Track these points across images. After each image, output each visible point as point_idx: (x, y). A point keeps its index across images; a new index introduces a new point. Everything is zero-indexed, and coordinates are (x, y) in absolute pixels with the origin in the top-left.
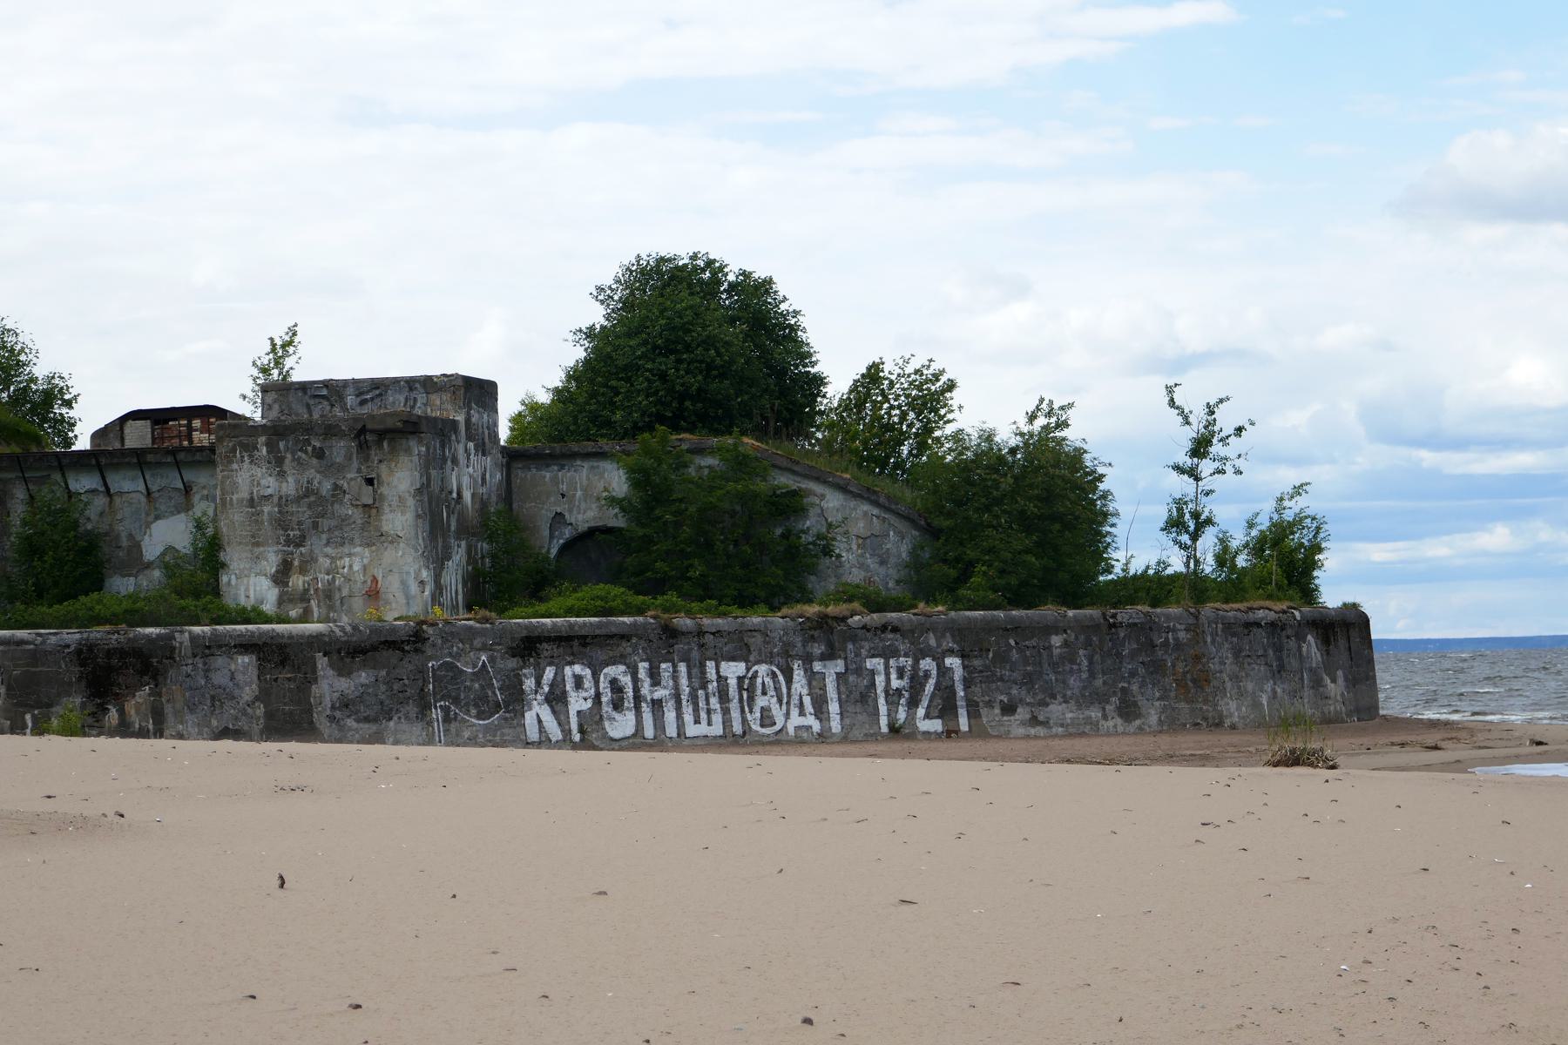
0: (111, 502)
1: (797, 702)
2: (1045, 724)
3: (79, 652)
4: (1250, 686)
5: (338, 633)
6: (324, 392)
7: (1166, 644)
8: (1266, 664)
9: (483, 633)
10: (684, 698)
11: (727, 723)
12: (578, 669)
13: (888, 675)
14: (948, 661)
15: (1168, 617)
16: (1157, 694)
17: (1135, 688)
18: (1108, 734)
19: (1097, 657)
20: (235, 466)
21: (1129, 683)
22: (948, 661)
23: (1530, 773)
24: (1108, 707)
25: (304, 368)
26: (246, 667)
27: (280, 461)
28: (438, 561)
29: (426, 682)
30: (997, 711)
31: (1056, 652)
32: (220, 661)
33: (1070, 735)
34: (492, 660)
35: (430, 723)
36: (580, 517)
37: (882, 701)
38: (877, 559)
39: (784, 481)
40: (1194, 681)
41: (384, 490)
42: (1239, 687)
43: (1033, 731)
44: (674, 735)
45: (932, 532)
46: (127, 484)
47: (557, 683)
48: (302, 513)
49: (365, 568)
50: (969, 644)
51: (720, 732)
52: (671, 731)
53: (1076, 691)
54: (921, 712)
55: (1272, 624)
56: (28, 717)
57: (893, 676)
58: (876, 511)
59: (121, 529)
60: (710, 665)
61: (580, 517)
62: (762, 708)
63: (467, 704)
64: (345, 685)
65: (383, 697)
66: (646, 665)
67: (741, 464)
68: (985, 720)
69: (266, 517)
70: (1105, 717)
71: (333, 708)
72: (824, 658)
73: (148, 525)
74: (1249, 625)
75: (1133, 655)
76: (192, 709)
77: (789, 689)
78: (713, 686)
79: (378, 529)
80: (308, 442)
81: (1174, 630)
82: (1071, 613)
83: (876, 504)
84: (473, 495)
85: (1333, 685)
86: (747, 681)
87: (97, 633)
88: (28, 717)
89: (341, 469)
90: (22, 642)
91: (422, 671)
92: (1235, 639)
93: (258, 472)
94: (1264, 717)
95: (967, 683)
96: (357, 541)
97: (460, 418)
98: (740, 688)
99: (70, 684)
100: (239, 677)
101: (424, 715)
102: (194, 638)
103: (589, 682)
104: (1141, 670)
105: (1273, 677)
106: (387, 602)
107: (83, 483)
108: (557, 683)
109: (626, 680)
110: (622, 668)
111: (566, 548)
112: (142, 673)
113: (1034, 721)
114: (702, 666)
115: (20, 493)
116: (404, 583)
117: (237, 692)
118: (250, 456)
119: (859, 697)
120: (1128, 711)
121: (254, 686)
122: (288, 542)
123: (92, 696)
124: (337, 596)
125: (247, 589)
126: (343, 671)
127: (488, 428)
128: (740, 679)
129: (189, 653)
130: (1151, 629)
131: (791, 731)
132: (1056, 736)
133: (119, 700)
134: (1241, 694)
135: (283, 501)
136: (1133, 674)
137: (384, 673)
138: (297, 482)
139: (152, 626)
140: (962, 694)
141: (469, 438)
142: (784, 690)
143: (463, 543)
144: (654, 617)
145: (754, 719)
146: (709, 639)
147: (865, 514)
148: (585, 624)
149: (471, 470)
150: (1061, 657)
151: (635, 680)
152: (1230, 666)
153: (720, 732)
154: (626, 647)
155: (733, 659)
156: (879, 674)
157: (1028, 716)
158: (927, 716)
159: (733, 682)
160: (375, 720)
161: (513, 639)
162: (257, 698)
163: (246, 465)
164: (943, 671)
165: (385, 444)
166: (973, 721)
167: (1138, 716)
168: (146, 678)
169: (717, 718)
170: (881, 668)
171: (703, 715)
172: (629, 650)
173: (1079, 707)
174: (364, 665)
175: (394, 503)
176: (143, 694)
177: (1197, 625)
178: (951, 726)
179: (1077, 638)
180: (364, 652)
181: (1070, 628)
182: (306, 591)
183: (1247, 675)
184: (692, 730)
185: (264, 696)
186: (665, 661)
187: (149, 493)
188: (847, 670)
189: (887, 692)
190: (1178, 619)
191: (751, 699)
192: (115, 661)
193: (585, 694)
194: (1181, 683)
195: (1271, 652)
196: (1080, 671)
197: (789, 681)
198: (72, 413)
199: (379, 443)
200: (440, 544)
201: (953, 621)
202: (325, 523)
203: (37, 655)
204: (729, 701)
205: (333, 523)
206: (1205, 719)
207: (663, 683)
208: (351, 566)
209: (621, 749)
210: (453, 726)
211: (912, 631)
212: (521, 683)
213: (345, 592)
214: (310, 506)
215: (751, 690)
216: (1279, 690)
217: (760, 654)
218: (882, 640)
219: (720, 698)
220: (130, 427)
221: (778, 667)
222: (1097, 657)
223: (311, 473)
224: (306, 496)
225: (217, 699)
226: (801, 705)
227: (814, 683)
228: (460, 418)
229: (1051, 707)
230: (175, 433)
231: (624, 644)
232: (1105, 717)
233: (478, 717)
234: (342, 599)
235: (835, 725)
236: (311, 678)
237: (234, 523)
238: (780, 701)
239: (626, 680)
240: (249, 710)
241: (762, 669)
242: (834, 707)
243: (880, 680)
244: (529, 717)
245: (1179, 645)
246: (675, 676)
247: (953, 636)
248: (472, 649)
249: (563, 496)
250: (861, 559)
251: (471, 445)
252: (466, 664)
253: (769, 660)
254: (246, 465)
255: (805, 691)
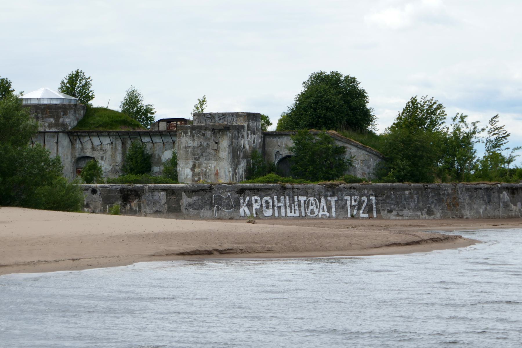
0: (153, 145)
1: (322, 208)
2: (402, 216)
3: (120, 190)
4: (475, 207)
5: (188, 187)
6: (210, 116)
7: (444, 194)
8: (483, 200)
9: (229, 187)
10: (287, 206)
11: (300, 213)
12: (256, 197)
13: (351, 201)
14: (371, 198)
15: (445, 186)
16: (440, 208)
17: (433, 206)
18: (423, 219)
19: (420, 197)
20: (182, 138)
21: (431, 205)
22: (371, 198)
23: (285, 227)
24: (423, 212)
25: (208, 109)
26: (163, 195)
27: (193, 137)
28: (235, 166)
29: (212, 200)
30: (386, 212)
31: (407, 196)
32: (156, 193)
33: (410, 219)
34: (231, 194)
35: (213, 211)
36: (284, 152)
37: (349, 209)
38: (366, 167)
40: (453, 205)
41: (220, 145)
42: (471, 207)
43: (398, 218)
44: (284, 216)
45: (383, 158)
46: (158, 140)
48: (199, 151)
49: (215, 167)
51: (298, 215)
52: (283, 214)
53: (413, 207)
54: (361, 211)
55: (487, 189)
56: (107, 206)
57: (353, 201)
58: (366, 153)
59: (156, 153)
60: (296, 197)
61: (284, 152)
62: (256, 209)
63: (224, 206)
64: (190, 200)
65: (200, 203)
66: (276, 197)
67: (327, 140)
68: (382, 214)
69: (189, 152)
70: (422, 214)
71: (186, 206)
72: (331, 196)
73: (163, 152)
74: (476, 189)
75: (433, 197)
76: (148, 205)
77: (320, 204)
78: (296, 203)
79: (218, 156)
80: (201, 131)
81: (447, 190)
82: (413, 185)
83: (366, 151)
84: (249, 147)
85: (515, 207)
86: (307, 202)
87: (125, 185)
88: (107, 206)
89: (209, 139)
90: (106, 187)
91: (211, 197)
92: (470, 193)
93: (188, 139)
94: (481, 216)
95: (377, 204)
96: (213, 159)
97: (245, 125)
98: (305, 203)
99: (118, 198)
100: (161, 197)
101: (211, 209)
102: (149, 187)
103: (259, 201)
104: (435, 201)
105: (486, 204)
106: (220, 177)
107: (146, 140)
109: (270, 201)
110: (269, 197)
111: (281, 161)
112: (136, 196)
113: (398, 215)
114: (293, 197)
115: (129, 142)
116: (225, 171)
117: (160, 201)
118: (186, 135)
119: (342, 207)
120: (430, 212)
121: (165, 200)
122: (195, 159)
123: (124, 201)
124: (207, 175)
125: (184, 172)
126: (189, 197)
127: (256, 127)
128: (305, 201)
129: (148, 191)
130: (439, 189)
131: (320, 215)
132: (405, 219)
133: (130, 202)
134: (471, 209)
135: (194, 148)
136: (432, 202)
137: (200, 197)
138: (198, 142)
139: (138, 184)
140: (375, 207)
141: (248, 130)
142: (318, 204)
143: (245, 160)
144: (280, 184)
146: (296, 190)
147: (363, 154)
148: (259, 185)
149: (249, 139)
150: (408, 197)
151: (273, 201)
153: (298, 215)
154: (271, 192)
155: (303, 196)
156: (348, 200)
157: (396, 214)
158: (363, 213)
159: (302, 202)
160: (198, 209)
161: (237, 189)
162: (166, 203)
163: (185, 137)
164: (369, 200)
165: (221, 133)
166: (378, 215)
167: (433, 214)
168: (137, 197)
169: (297, 212)
170: (349, 199)
171: (293, 211)
172: (271, 193)
173: (413, 211)
174: (195, 195)
175: (223, 149)
176: (136, 201)
177: (455, 189)
178: (371, 216)
179: (414, 192)
180: (195, 192)
181: (412, 189)
182: (199, 173)
183: (474, 203)
184: (289, 214)
185: (167, 202)
186: (282, 196)
187: (163, 143)
188: (338, 199)
189: (351, 206)
190: (449, 187)
191: (308, 207)
192: (129, 193)
193: (258, 204)
194: (449, 205)
195: (485, 197)
196: (414, 201)
197: (320, 202)
198: (154, 116)
199: (219, 132)
200: (236, 161)
201: (373, 186)
202: (205, 154)
203: (110, 191)
204: (301, 207)
205: (207, 154)
206: (456, 216)
207: (281, 202)
208: (211, 166)
209: (268, 219)
210: (220, 211)
211: (360, 189)
212: (239, 201)
213: (209, 173)
214: (201, 149)
215: (308, 204)
216: (488, 208)
217: (311, 194)
218: (350, 191)
219: (298, 206)
220: (161, 123)
221: (317, 198)
222: (420, 197)
223: (201, 140)
224: (200, 146)
225: (155, 203)
226: (323, 209)
227: (328, 203)
228: (245, 125)
229: (404, 211)
230: (173, 126)
231: (270, 191)
232: (422, 214)
233: (227, 209)
234: (209, 175)
235: (334, 214)
236: (180, 198)
237: (180, 154)
238: (317, 208)
239: (270, 201)
240: (163, 206)
241: (312, 199)
242: (334, 210)
243: (349, 203)
244: (241, 210)
245: (448, 194)
246: (285, 200)
247: (373, 191)
248: (226, 191)
249: (279, 146)
250: (362, 167)
251: (249, 132)
252: (224, 195)
253: (314, 196)
254: (185, 137)
255: (325, 205)
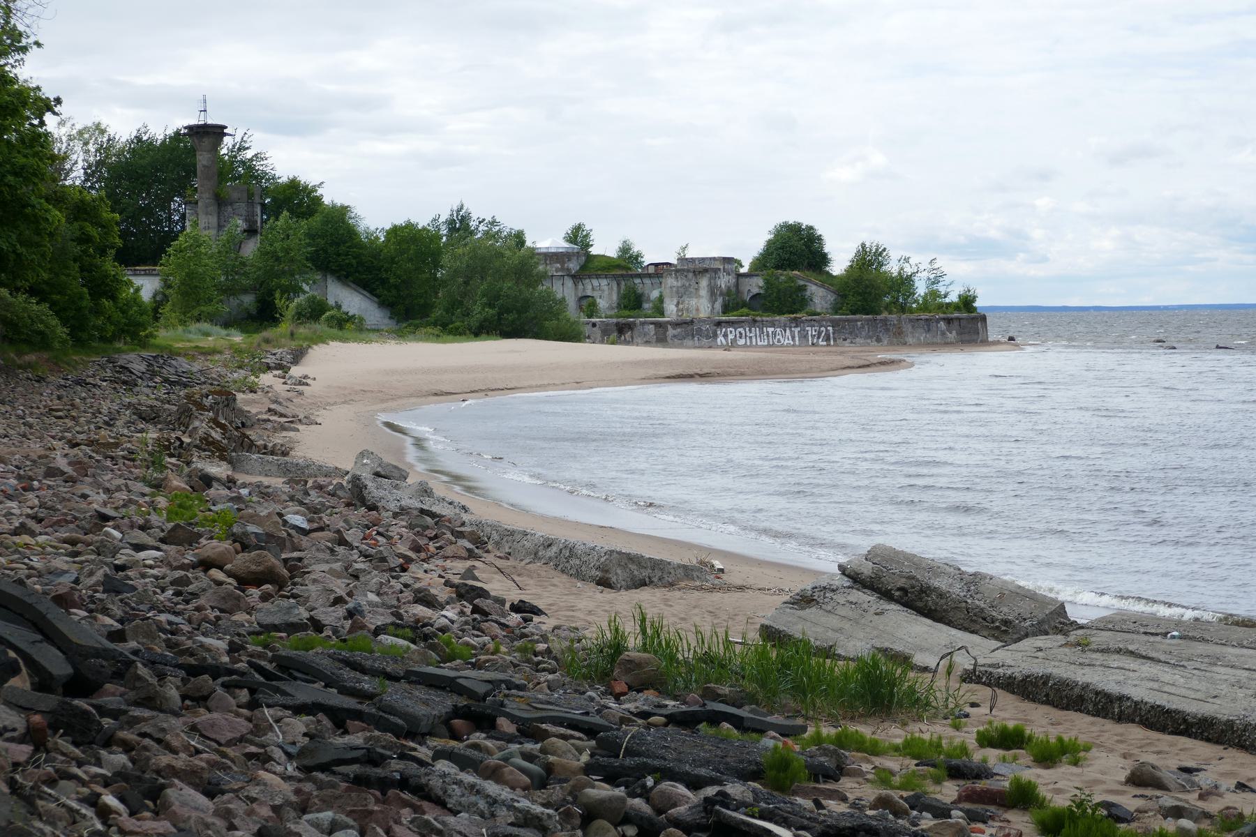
25: (690, 254)
28: (713, 302)
39: (801, 283)
46: (647, 281)
47: (726, 332)
48: (682, 290)
50: (835, 324)
59: (646, 292)
97: (722, 267)
107: (637, 281)
108: (726, 332)
109: (743, 332)
111: (751, 298)
119: (804, 336)
120: (879, 340)
126: (674, 329)
135: (678, 287)
145: (776, 341)
152: (910, 329)
164: (827, 330)
184: (759, 343)
185: (656, 334)
203: (607, 325)
228: (722, 267)
235: (797, 343)
237: (666, 293)
239: (743, 332)
242: (797, 339)
